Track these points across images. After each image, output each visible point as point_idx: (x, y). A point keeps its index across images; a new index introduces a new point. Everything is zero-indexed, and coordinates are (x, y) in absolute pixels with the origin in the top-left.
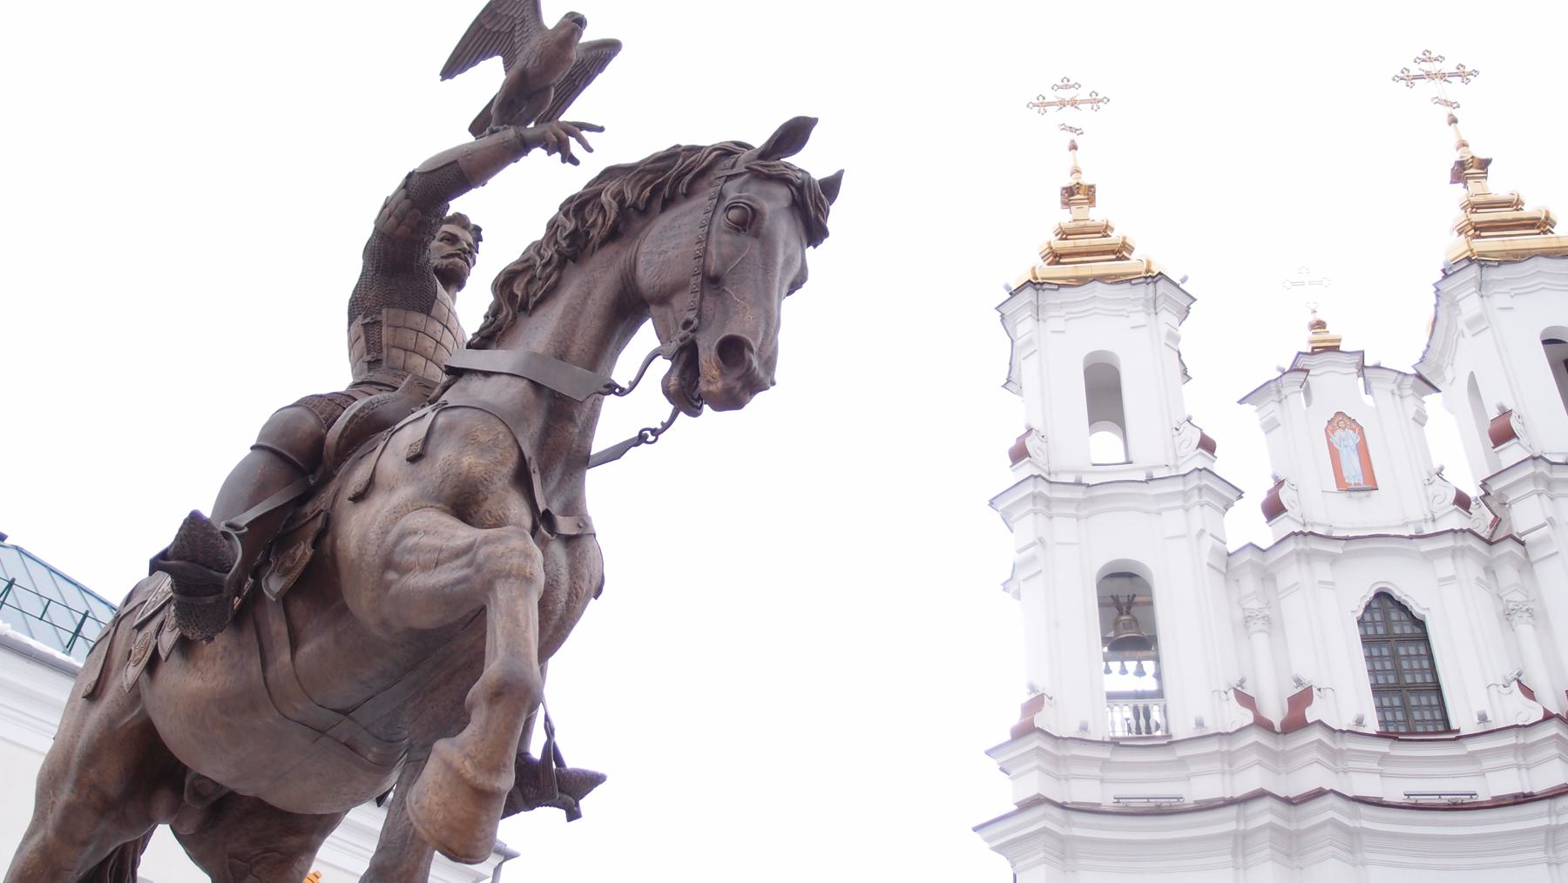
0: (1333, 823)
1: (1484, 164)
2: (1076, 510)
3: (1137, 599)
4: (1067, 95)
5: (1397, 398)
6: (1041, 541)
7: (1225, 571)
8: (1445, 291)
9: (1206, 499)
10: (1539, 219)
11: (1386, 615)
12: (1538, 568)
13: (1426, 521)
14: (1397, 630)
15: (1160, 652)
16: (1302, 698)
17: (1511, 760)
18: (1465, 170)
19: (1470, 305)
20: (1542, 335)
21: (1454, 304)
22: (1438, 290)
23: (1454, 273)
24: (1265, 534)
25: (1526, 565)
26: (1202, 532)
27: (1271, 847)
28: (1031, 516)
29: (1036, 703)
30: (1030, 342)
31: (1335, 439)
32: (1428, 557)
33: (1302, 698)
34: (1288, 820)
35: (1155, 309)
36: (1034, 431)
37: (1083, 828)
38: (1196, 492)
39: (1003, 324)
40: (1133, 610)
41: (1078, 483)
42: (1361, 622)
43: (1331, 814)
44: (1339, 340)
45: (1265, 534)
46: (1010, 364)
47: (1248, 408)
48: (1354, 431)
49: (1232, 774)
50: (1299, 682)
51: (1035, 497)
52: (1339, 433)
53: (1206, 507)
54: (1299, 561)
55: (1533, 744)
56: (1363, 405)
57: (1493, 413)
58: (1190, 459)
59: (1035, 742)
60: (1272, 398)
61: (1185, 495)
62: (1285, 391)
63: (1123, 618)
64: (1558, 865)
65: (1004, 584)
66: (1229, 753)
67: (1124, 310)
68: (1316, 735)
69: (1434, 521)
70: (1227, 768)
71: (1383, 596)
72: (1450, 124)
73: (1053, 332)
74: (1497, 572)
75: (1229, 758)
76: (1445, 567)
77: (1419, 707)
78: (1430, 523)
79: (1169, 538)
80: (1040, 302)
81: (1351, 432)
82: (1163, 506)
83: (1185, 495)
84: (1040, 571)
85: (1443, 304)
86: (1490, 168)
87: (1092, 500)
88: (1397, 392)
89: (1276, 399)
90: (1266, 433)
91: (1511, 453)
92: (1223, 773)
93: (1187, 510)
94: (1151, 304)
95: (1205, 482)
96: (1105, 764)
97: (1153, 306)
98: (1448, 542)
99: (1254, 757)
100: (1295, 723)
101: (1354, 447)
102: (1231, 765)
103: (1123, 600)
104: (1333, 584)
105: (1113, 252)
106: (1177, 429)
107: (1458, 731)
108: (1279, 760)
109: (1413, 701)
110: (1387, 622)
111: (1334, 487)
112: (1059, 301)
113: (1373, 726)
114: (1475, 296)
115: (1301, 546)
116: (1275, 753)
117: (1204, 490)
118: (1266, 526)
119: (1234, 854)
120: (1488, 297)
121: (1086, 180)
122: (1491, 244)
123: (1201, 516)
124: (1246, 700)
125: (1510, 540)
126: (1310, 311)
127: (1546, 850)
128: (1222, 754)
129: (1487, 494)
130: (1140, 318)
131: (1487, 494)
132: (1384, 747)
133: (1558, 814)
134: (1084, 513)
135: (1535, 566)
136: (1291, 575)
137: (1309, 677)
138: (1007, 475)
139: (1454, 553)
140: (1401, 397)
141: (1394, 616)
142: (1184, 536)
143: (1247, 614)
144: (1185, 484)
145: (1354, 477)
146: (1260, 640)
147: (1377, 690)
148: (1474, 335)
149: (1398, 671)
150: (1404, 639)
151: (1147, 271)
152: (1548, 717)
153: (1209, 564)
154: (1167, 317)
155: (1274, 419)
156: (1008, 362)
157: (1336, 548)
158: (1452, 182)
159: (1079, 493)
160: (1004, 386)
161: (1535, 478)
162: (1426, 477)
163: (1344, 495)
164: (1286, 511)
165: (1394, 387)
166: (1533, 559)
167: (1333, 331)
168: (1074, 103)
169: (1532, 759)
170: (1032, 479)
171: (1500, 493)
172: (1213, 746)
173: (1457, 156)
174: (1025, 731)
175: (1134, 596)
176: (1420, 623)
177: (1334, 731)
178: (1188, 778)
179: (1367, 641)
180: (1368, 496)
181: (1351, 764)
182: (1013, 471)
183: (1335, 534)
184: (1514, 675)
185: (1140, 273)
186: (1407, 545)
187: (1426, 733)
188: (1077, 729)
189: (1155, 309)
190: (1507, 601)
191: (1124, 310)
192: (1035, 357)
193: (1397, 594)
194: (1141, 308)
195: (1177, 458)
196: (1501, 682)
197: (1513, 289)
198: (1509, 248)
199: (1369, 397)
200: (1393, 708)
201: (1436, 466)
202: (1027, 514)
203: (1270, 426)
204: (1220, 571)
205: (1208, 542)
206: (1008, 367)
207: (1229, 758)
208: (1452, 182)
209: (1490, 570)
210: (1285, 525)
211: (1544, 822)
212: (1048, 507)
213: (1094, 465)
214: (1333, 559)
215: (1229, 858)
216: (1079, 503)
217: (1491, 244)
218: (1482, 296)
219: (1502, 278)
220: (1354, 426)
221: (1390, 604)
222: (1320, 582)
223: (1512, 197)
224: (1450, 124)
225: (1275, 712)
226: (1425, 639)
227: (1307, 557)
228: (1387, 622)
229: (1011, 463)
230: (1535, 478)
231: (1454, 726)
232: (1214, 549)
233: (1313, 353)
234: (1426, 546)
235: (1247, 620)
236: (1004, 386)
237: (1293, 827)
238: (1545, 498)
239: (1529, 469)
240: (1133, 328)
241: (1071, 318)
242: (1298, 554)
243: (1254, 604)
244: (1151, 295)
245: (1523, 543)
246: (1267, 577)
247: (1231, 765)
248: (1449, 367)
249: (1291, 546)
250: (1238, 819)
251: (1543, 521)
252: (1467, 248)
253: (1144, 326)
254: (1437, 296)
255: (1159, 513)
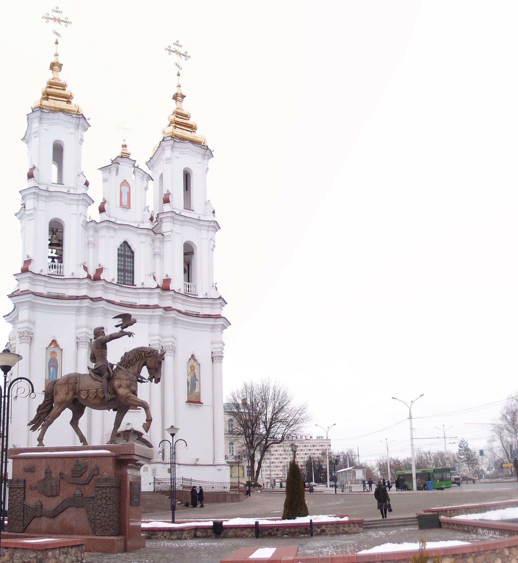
0: (103, 307)
1: (183, 97)
2: (46, 199)
3: (59, 230)
4: (57, 16)
5: (142, 180)
6: (35, 208)
7: (85, 227)
8: (163, 145)
9: (84, 203)
10: (193, 126)
11: (125, 248)
12: (165, 243)
13: (141, 222)
14: (127, 253)
15: (63, 248)
16: (100, 271)
17: (147, 296)
18: (177, 97)
19: (168, 153)
20: (185, 168)
21: (163, 150)
22: (160, 143)
23: (167, 140)
24: (97, 217)
25: (162, 241)
26: (81, 214)
27: (86, 311)
28: (33, 199)
29: (28, 262)
30: (37, 132)
31: (122, 189)
32: (140, 234)
33: (100, 271)
34: (92, 305)
35: (78, 127)
36: (36, 168)
37: (40, 301)
38: (82, 200)
39: (28, 121)
40: (57, 233)
41: (47, 191)
42: (118, 249)
43: (102, 305)
44: (129, 154)
45: (97, 217)
46: (26, 133)
47: (100, 172)
48: (128, 187)
49: (79, 289)
50: (100, 265)
51: (34, 193)
52: (124, 187)
53: (84, 206)
54: (106, 229)
55: (153, 293)
56: (133, 179)
57: (165, 192)
58: (81, 188)
59: (28, 275)
60: (107, 171)
61: (78, 200)
62: (112, 169)
63: (54, 236)
64: (151, 324)
65: (15, 214)
66: (79, 284)
67: (68, 126)
68: (102, 283)
69: (143, 223)
70: (78, 288)
71: (125, 242)
72: (178, 75)
73: (45, 129)
74: (155, 242)
75: (79, 285)
76: (143, 238)
77: (128, 277)
78: (142, 223)
79: (72, 214)
80: (42, 116)
81: (127, 187)
82: (72, 203)
83: (78, 200)
84: (33, 219)
85: (160, 149)
86: (185, 99)
87: (51, 196)
88: (142, 178)
89: (109, 172)
90: (103, 182)
91: (167, 208)
92: (77, 289)
93: (78, 205)
94: (77, 125)
95: (85, 198)
96: (46, 282)
97: (77, 126)
98: (145, 232)
99: (86, 286)
100: (97, 278)
101: (127, 193)
102: (79, 287)
103: (55, 230)
104: (113, 237)
105: (66, 98)
106: (79, 176)
107: (136, 285)
108: (91, 287)
109: (127, 274)
110: (125, 250)
111: (119, 206)
112: (48, 117)
113: (115, 282)
114: (170, 150)
115: (108, 225)
116: (91, 285)
117: (84, 200)
118: (99, 214)
119: (76, 312)
120: (173, 151)
121: (61, 62)
122: (179, 132)
123: (81, 208)
124: (86, 269)
125: (161, 234)
126: (123, 140)
127: (149, 320)
128: (77, 283)
129: (158, 217)
130: (72, 130)
131: (158, 217)
132: (117, 288)
133: (154, 312)
134: (48, 200)
135: (164, 242)
136: (103, 232)
137: (103, 265)
138: (26, 184)
139: (146, 235)
140: (143, 180)
141: (127, 249)
142: (76, 214)
143: (89, 242)
144: (79, 197)
145: (125, 203)
146: (91, 250)
147: (119, 270)
148: (166, 163)
149: (124, 265)
150: (128, 256)
151: (78, 112)
152: (158, 287)
153: (82, 225)
154: (80, 131)
155: (107, 179)
156: (25, 131)
157: (116, 227)
158: (172, 99)
159: (47, 194)
160: (22, 140)
161: (171, 217)
162: (144, 208)
163: (121, 208)
164: (105, 211)
165: (142, 176)
166: (164, 240)
167: (129, 150)
168: (59, 21)
169: (152, 296)
170: (35, 187)
171: (161, 218)
172: (75, 281)
173: (175, 92)
174: (25, 270)
175: (58, 229)
176: (133, 253)
177: (107, 282)
178: (67, 289)
179: (119, 255)
180: (127, 210)
181: (109, 291)
182: (28, 181)
183: (118, 222)
184: (152, 273)
185: (75, 111)
186: (135, 229)
187: (128, 285)
188: (40, 271)
189: (78, 127)
190: (156, 251)
191: (68, 126)
192: (38, 138)
193: (129, 243)
194: (74, 126)
195: (77, 186)
196: (149, 274)
197: (180, 151)
198: (183, 135)
199: (133, 175)
200: (121, 276)
201: (147, 205)
202: (32, 198)
203: (105, 180)
204: (84, 227)
205: (83, 218)
206: (25, 134)
207: (79, 285)
208: (172, 99)
209: (153, 241)
210: (104, 216)
211: (151, 314)
212: (38, 197)
213: (53, 183)
214: (115, 229)
215: (75, 312)
216: (47, 197)
217: (179, 132)
218: (172, 151)
219: (179, 146)
220: (128, 186)
221: (126, 245)
222: (111, 236)
223: (188, 114)
224: (178, 75)
225: (92, 273)
226: (133, 257)
227: (108, 228)
228: (125, 250)
229: (27, 178)
230: (171, 217)
231: (135, 284)
232: (84, 220)
233: (122, 157)
234: (140, 231)
235: (89, 243)
236: (22, 140)
237: (93, 307)
238: (172, 223)
239: (170, 214)
240: (70, 133)
241: (51, 125)
242: (106, 226)
243: (91, 239)
244: (78, 122)
245: (163, 235)
246: (96, 231)
247: (79, 287)
248: (156, 167)
249: (105, 224)
250: (79, 303)
251: (170, 230)
252: (172, 131)
253: (73, 134)
254: (160, 145)
255: (70, 205)
